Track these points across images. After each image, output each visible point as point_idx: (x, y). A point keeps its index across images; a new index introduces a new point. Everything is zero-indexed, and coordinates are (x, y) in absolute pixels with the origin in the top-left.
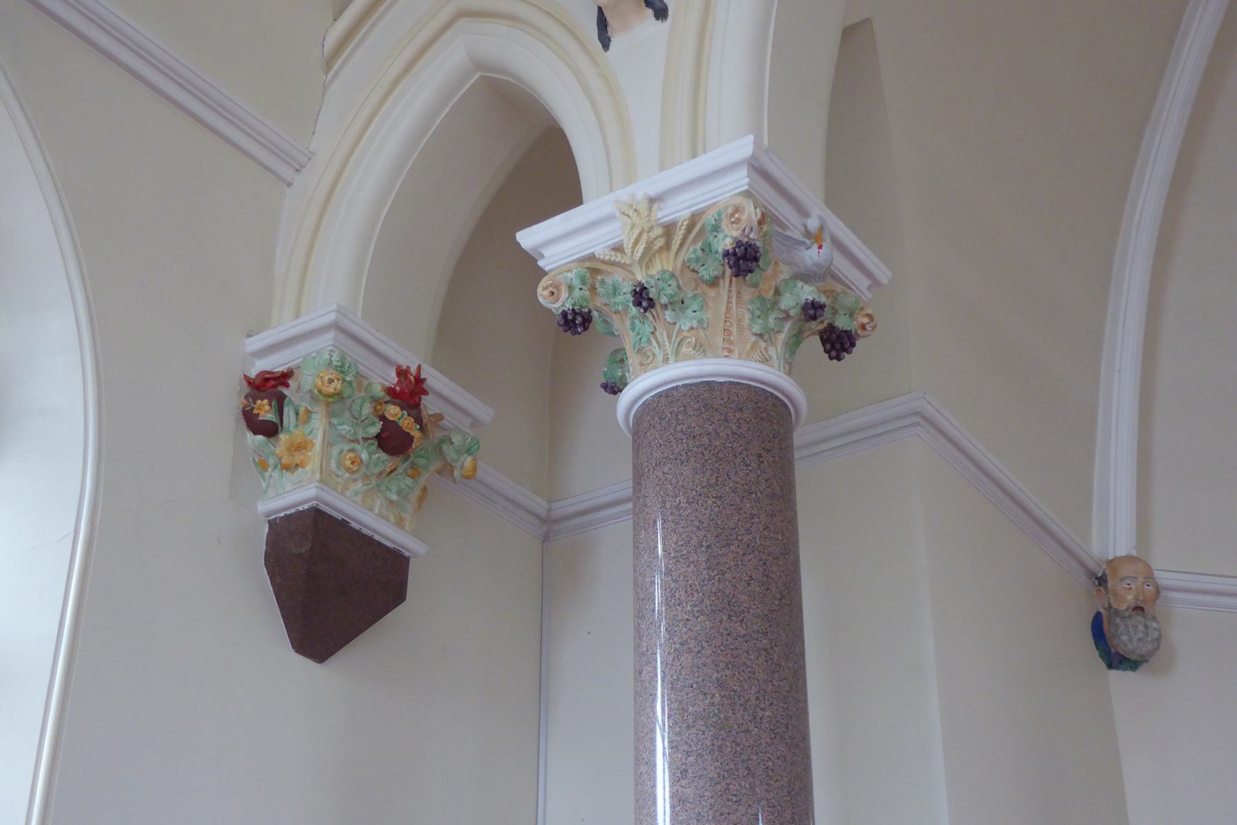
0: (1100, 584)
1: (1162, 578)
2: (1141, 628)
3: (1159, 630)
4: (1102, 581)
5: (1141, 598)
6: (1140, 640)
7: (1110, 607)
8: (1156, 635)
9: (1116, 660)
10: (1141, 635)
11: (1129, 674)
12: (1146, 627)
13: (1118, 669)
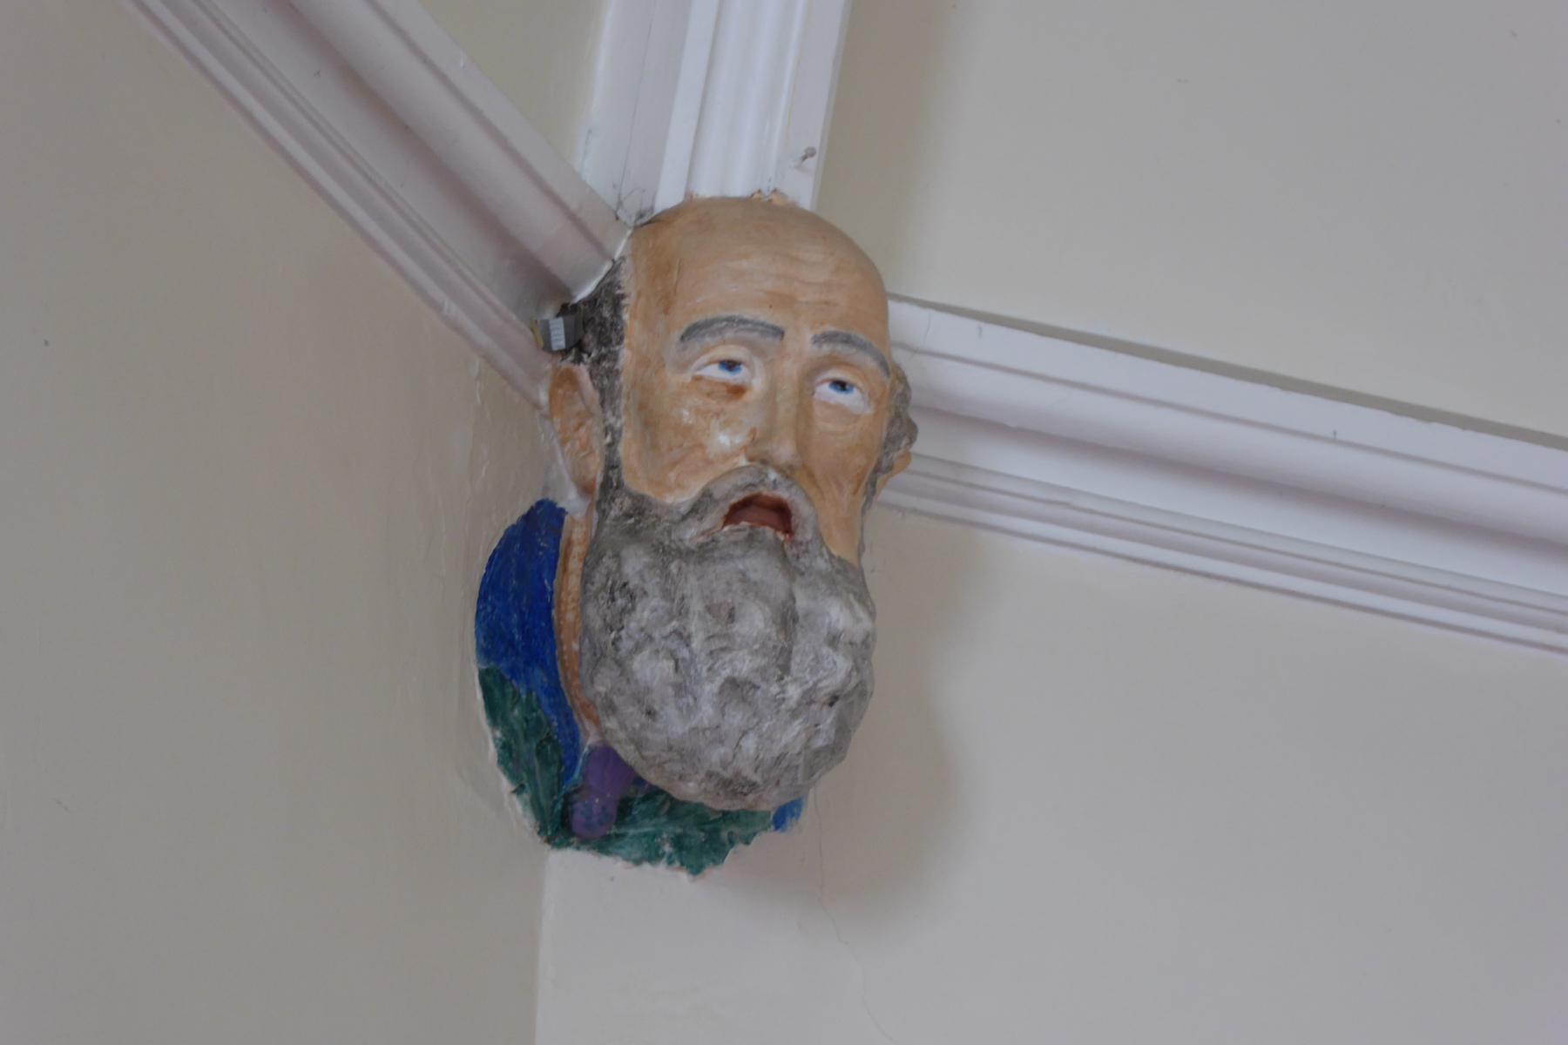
0: (576, 347)
1: (948, 349)
2: (755, 621)
3: (862, 651)
4: (590, 327)
5: (784, 451)
6: (736, 688)
7: (609, 487)
8: (839, 667)
9: (590, 792)
10: (744, 664)
11: (662, 887)
12: (787, 620)
13: (603, 844)
